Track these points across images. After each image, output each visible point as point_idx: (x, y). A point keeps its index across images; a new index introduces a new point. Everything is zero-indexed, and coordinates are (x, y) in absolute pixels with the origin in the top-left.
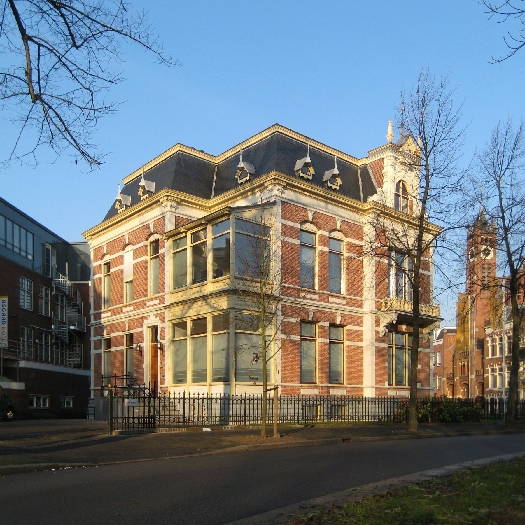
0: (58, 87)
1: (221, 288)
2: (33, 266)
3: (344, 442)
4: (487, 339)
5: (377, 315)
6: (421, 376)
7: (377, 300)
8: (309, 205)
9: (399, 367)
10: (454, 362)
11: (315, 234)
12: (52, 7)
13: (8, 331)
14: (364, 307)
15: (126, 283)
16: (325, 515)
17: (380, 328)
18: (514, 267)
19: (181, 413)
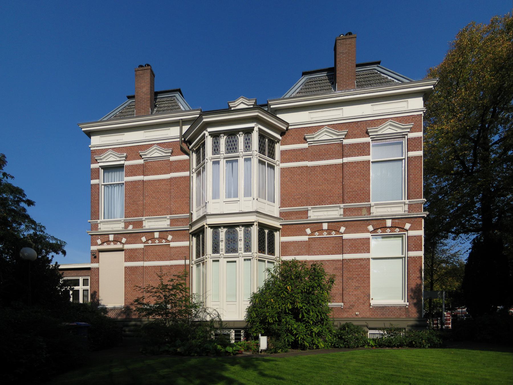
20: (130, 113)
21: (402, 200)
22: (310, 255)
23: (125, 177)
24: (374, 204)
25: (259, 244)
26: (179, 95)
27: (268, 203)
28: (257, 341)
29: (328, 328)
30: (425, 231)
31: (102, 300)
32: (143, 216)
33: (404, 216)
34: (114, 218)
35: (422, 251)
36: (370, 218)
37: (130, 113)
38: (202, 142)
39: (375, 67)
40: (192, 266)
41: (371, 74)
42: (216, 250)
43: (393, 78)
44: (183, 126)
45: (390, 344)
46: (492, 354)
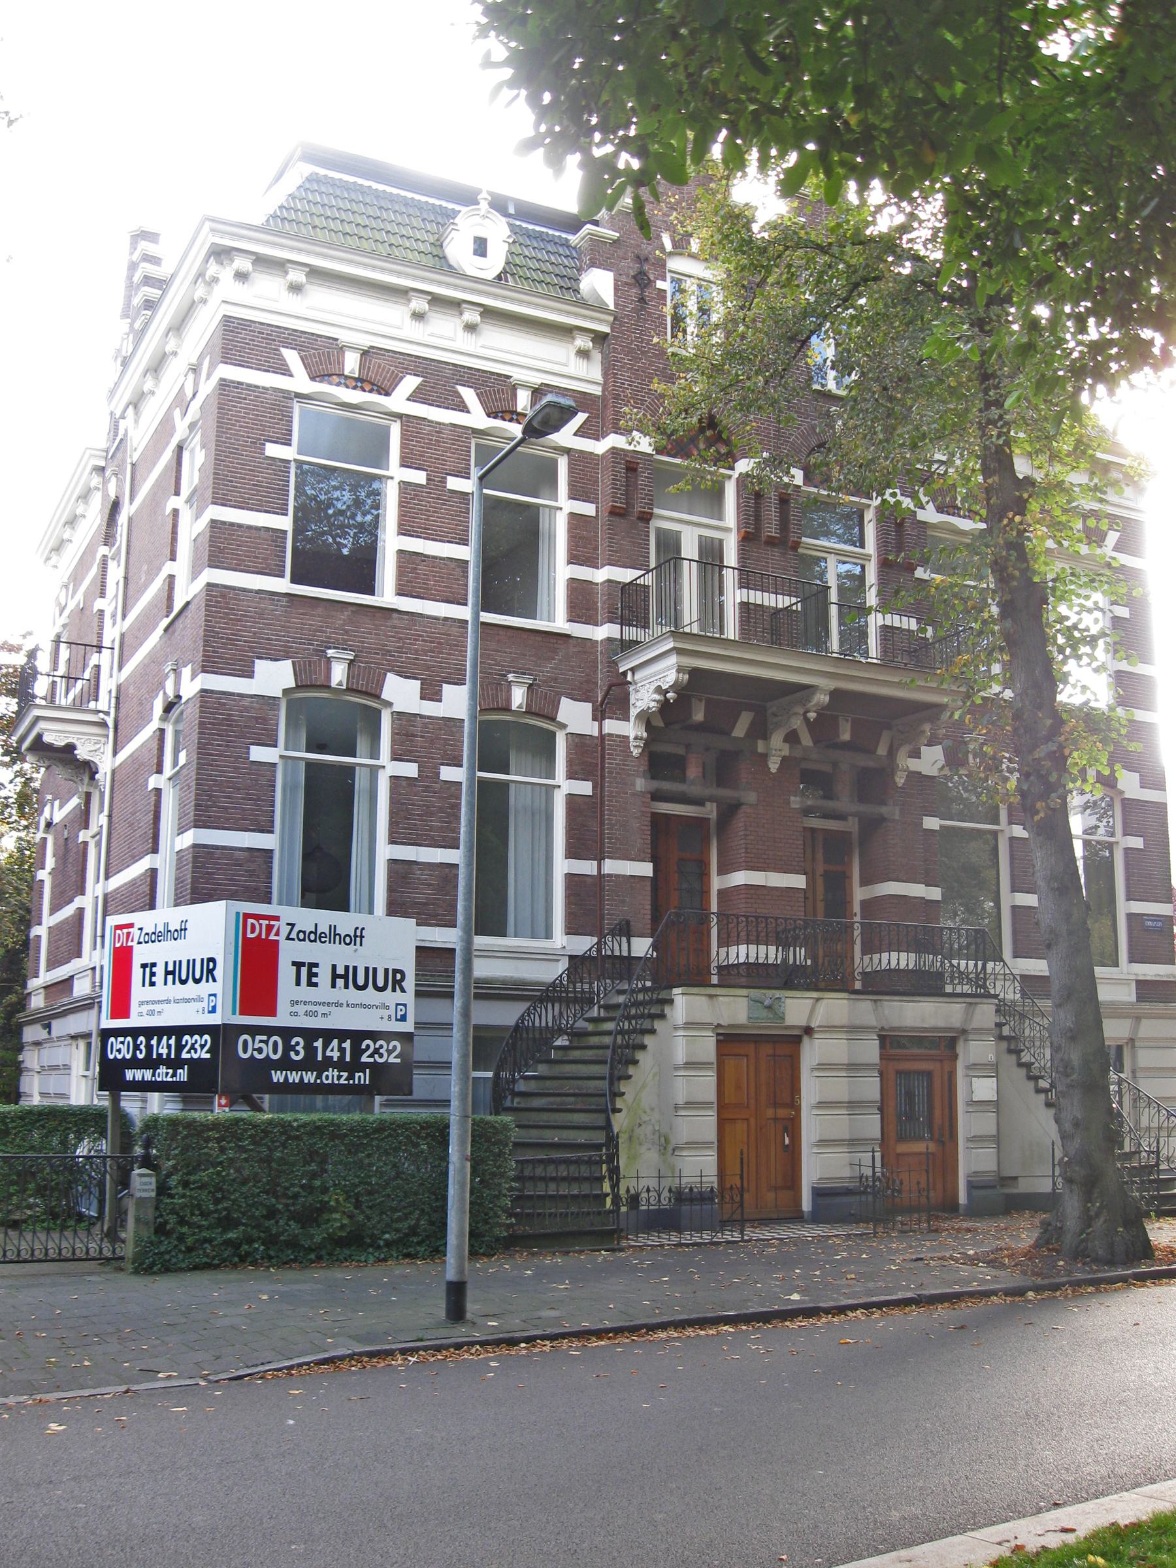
0: (125, 394)
1: (1016, 1285)
2: (6, 1233)
3: (316, 985)
4: (1065, 669)
5: (830, 804)
6: (348, 382)
7: (550, 727)
8: (492, 432)
9: (822, 985)
10: (183, 321)
11: (155, 850)
12: (815, 995)
13: (793, 1126)
14: (256, 674)
15: (821, 1067)
16: (846, 51)
17: (880, 622)
18: (663, 177)
19: (529, 801)
20: (585, 1171)
21: (548, 935)
22: (618, 736)
23: (411, 1093)
24: (708, 804)
25: (391, 818)
26: (978, 1077)
27: (108, 674)
28: (130, 1267)
29: (1080, 239)
30: (296, 520)
31: (531, 144)
32: (419, 994)
33: (318, 249)
34: (446, 1103)
35: (286, 515)
36: (470, 1092)
37: (585, 1171)
38: (450, 206)
39: (122, 519)
40: (87, 1073)
41: (556, 275)
42: (102, 967)
43: (84, 469)
44: (558, 719)
45: (397, 1230)
46: (1040, 1191)
